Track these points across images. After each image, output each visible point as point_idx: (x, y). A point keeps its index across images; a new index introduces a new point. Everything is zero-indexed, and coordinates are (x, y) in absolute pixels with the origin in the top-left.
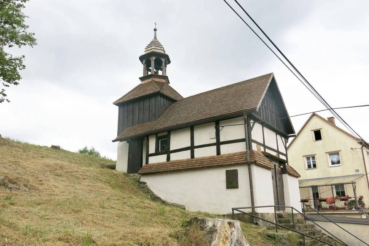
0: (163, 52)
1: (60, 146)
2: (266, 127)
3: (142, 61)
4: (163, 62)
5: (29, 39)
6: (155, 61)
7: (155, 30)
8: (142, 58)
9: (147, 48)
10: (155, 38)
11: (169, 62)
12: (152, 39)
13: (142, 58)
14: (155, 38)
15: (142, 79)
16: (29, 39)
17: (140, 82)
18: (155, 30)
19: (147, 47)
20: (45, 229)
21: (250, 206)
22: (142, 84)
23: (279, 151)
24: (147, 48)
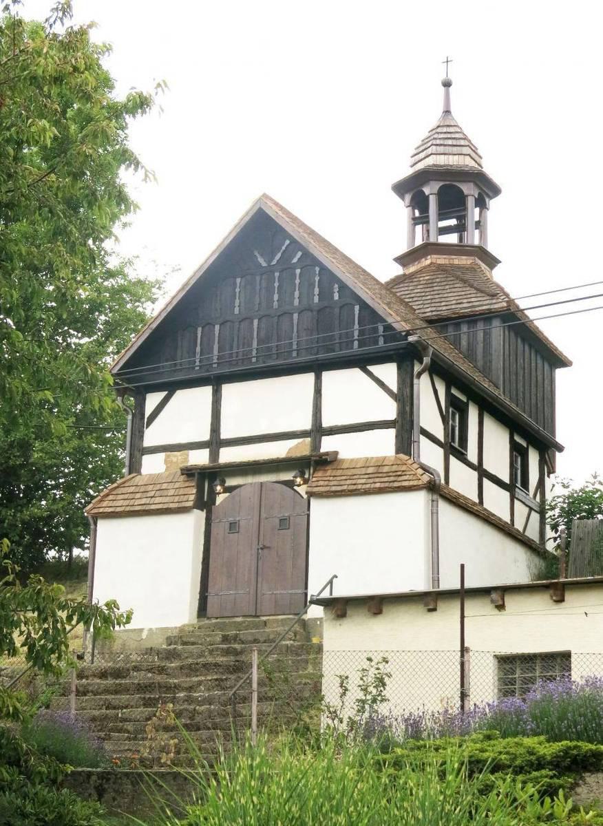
0: (469, 162)
1: (336, 453)
2: (397, 437)
3: (402, 196)
4: (467, 196)
5: (142, 115)
6: (441, 194)
7: (447, 84)
8: (401, 188)
9: (416, 155)
10: (447, 112)
11: (495, 191)
12: (433, 117)
13: (401, 188)
14: (447, 112)
15: (403, 260)
16: (142, 115)
17: (398, 270)
18: (447, 84)
19: (415, 152)
20: (134, 724)
21: (468, 585)
22: (404, 275)
23: (485, 467)
24: (416, 155)
